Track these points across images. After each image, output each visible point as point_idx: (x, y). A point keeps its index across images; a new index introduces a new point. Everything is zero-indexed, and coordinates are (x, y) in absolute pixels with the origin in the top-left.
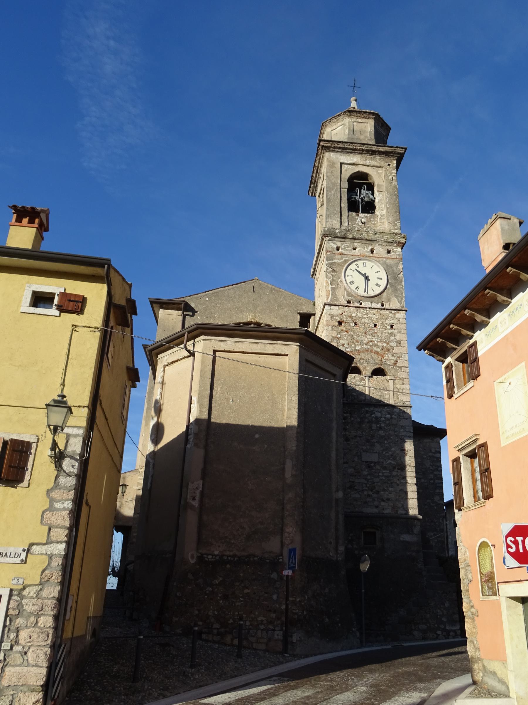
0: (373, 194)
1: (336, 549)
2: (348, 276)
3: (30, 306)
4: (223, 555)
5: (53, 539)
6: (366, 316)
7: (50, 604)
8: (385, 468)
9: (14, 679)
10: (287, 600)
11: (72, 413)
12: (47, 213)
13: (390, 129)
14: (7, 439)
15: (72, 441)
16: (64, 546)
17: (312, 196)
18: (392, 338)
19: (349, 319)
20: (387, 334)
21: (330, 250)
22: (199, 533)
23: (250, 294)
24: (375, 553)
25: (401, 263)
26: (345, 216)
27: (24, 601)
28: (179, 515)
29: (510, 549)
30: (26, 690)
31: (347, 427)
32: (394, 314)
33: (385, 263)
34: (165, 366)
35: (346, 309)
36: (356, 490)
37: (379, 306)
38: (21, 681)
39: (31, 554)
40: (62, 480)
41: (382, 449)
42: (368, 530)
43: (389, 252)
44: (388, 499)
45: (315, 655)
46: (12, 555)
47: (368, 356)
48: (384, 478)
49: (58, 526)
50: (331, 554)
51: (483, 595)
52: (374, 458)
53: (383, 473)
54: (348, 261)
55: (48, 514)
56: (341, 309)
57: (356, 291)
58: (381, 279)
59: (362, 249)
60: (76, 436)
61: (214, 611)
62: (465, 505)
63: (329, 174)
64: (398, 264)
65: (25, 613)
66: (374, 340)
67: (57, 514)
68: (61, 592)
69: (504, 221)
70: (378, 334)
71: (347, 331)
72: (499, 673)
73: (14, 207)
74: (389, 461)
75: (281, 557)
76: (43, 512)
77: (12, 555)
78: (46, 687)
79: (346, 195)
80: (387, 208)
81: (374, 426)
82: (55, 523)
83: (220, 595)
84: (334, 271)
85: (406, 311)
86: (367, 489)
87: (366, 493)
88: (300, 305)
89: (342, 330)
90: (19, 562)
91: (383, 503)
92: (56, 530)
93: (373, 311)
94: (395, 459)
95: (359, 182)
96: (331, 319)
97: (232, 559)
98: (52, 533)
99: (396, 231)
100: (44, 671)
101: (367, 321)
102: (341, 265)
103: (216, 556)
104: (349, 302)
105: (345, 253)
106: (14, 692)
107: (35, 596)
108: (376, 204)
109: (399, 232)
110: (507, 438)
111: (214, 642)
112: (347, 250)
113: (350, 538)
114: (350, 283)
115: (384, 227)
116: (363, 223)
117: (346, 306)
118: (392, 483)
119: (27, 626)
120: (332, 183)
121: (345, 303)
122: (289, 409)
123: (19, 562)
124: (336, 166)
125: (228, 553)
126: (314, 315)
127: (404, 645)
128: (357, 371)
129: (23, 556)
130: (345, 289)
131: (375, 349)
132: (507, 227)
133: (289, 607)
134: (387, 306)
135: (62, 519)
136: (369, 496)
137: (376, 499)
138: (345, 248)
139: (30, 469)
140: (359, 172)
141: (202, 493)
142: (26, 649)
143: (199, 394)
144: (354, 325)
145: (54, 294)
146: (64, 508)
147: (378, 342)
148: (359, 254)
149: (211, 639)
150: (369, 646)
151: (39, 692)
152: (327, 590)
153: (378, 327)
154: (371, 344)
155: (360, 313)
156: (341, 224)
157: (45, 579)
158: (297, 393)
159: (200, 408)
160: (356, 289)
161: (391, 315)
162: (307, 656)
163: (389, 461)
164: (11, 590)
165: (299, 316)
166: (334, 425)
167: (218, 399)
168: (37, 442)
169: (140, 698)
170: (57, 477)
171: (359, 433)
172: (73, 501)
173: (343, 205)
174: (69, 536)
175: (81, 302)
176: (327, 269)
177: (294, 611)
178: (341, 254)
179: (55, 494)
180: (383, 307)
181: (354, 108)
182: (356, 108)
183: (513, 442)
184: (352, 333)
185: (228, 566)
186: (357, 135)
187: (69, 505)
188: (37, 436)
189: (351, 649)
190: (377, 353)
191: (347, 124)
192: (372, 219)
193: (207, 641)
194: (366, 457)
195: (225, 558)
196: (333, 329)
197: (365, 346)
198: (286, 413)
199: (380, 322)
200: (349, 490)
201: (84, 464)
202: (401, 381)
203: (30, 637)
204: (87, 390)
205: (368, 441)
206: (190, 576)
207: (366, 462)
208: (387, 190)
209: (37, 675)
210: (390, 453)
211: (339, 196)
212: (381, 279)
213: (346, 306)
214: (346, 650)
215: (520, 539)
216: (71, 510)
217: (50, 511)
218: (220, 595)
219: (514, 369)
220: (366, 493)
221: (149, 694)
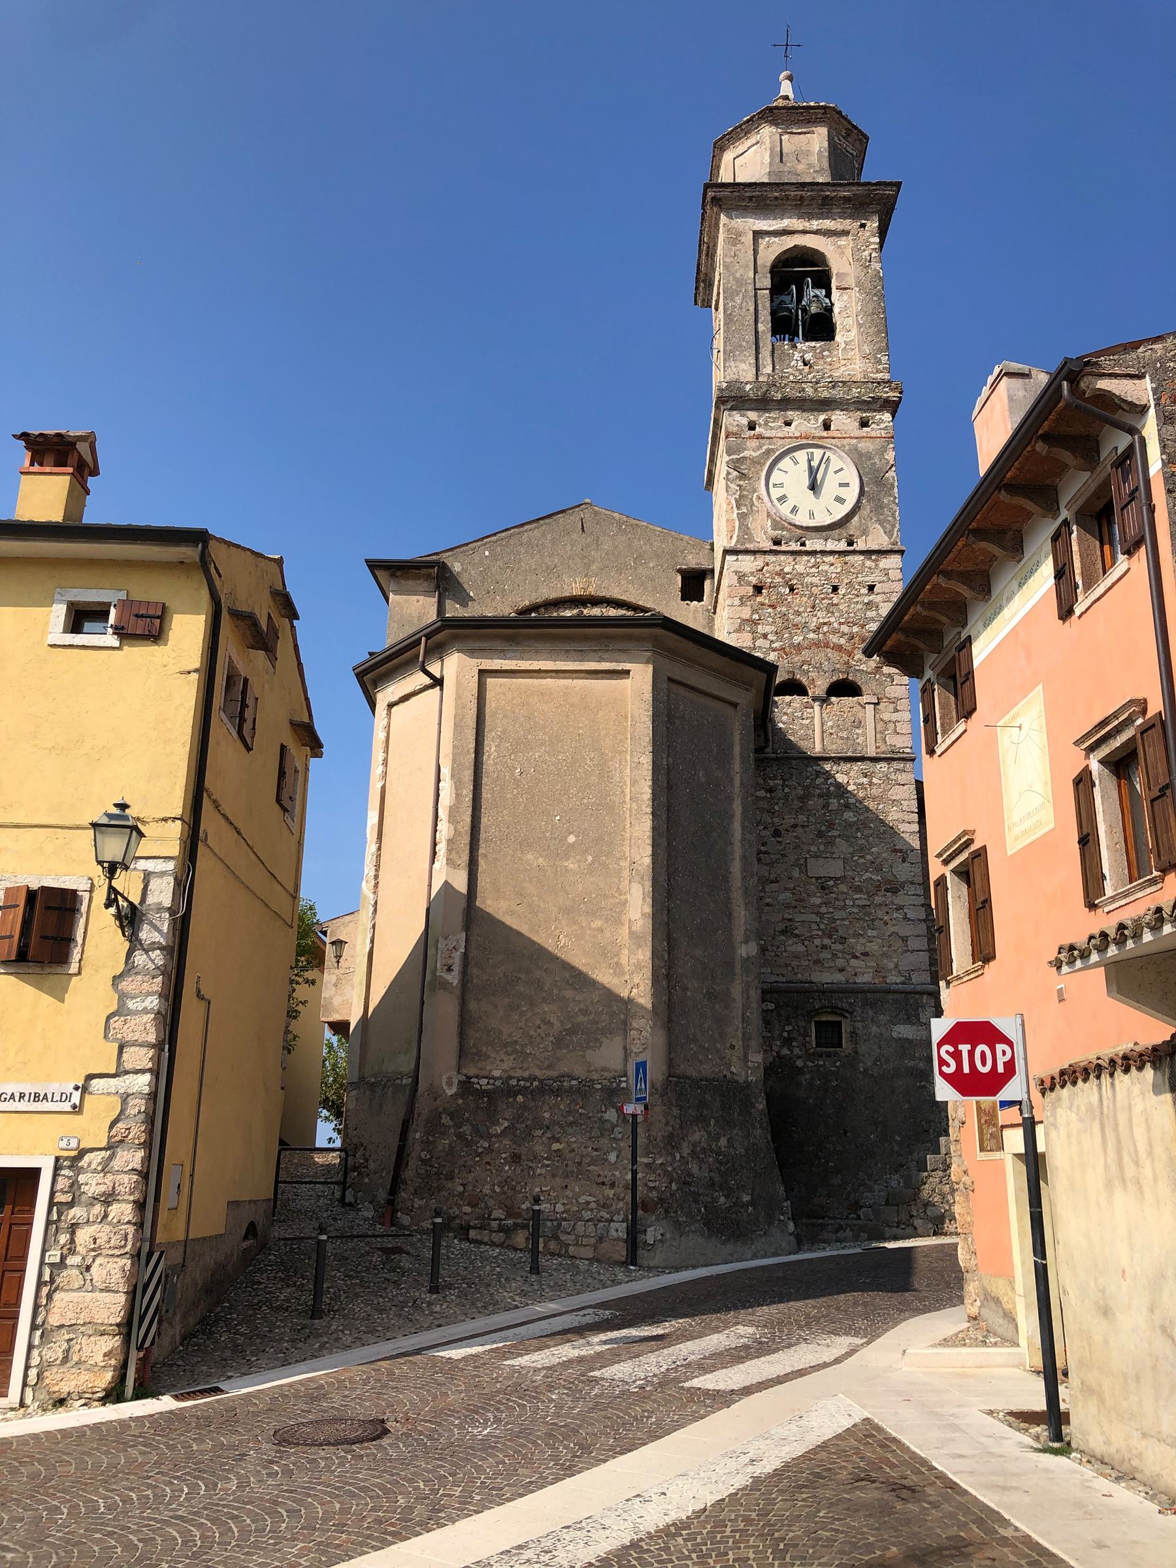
0: (829, 295)
1: (745, 1059)
2: (775, 485)
3: (65, 632)
4: (510, 1078)
5: (128, 1066)
6: (814, 570)
7: (126, 1181)
8: (858, 889)
9: (70, 1315)
10: (634, 1160)
11: (141, 835)
12: (90, 439)
13: (867, 139)
14: (35, 886)
15: (154, 884)
16: (147, 1078)
17: (703, 306)
18: (869, 614)
19: (778, 579)
20: (860, 606)
21: (735, 429)
22: (462, 1035)
23: (575, 536)
24: (838, 1064)
25: (892, 446)
26: (765, 353)
27: (82, 1178)
28: (423, 1003)
29: (944, 1069)
30: (90, 1332)
31: (776, 808)
32: (876, 560)
33: (856, 449)
34: (391, 706)
35: (771, 558)
36: (797, 936)
37: (842, 546)
38: (82, 1316)
39: (91, 1093)
40: (140, 958)
41: (851, 850)
42: (824, 1018)
43: (864, 424)
44: (866, 954)
45: (694, 1267)
46: (57, 1098)
47: (819, 656)
48: (856, 911)
49: (135, 1044)
50: (733, 1069)
51: (981, 1150)
52: (834, 868)
53: (854, 900)
54: (773, 451)
55: (116, 1023)
56: (760, 561)
57: (792, 516)
58: (847, 485)
59: (804, 424)
60: (162, 874)
61: (494, 1185)
62: (955, 974)
63: (728, 260)
64: (883, 450)
65: (84, 1198)
66: (832, 620)
67: (134, 1021)
68: (147, 1159)
69: (1017, 383)
70: (841, 607)
71: (773, 607)
72: (1004, 1300)
73: (24, 436)
74: (868, 875)
75: (624, 1079)
76: (109, 1018)
77: (57, 1098)
78: (126, 1328)
79: (768, 304)
80: (860, 326)
81: (834, 804)
82: (130, 1037)
83: (504, 1156)
84: (743, 476)
85: (902, 552)
86: (820, 933)
87: (817, 942)
88: (682, 552)
89: (763, 604)
90: (70, 1109)
91: (853, 962)
92: (132, 1049)
93: (830, 559)
94: (879, 870)
95: (798, 273)
96: (739, 582)
97: (528, 1084)
98: (125, 1056)
99: (879, 376)
100: (121, 1299)
101: (815, 580)
102: (757, 462)
103: (495, 1079)
104: (777, 542)
105: (768, 434)
106: (72, 1336)
107: (100, 1168)
108: (837, 317)
109: (887, 376)
110: (1016, 839)
111: (493, 1244)
112: (772, 428)
113: (785, 1034)
114: (779, 499)
115: (853, 369)
116: (805, 364)
117: (771, 552)
118: (873, 920)
119: (88, 1221)
120: (735, 279)
121: (768, 545)
122: (634, 783)
123: (70, 1109)
124: (743, 239)
125: (519, 1073)
126: (712, 571)
127: (891, 1245)
128: (795, 688)
129: (76, 1098)
130: (769, 515)
131: (834, 639)
132: (1021, 393)
133: (639, 1176)
134: (860, 545)
135: (143, 1027)
136: (824, 947)
137: (840, 955)
138: (766, 424)
139: (79, 939)
140: (795, 246)
141: (465, 956)
142: (89, 1261)
143: (454, 761)
144: (788, 590)
145: (109, 604)
146: (145, 1008)
147: (840, 624)
148: (797, 435)
149: (486, 1239)
150: (810, 1250)
151: (114, 1336)
152: (723, 1142)
153: (842, 591)
154: (825, 629)
155: (802, 565)
156: (757, 370)
157: (117, 1139)
158: (651, 749)
159: (456, 789)
160: (792, 512)
161: (868, 563)
162: (677, 1269)
163: (868, 875)
164: (57, 1159)
165: (679, 578)
166: (737, 807)
167: (491, 769)
168: (91, 891)
169: (317, 1346)
170: (129, 954)
171: (802, 818)
172: (160, 996)
173: (761, 327)
174: (157, 1060)
175: (158, 617)
176: (728, 473)
177: (651, 1184)
178: (759, 437)
179: (126, 985)
180: (851, 548)
181: (786, 98)
182: (791, 96)
183: (1023, 848)
184: (784, 609)
185: (520, 1098)
186: (790, 163)
187: (153, 1002)
188: (90, 879)
189: (775, 1255)
190: (839, 648)
191: (767, 141)
192: (826, 353)
193: (480, 1243)
194: (817, 868)
195: (513, 1082)
196: (742, 604)
197: (811, 635)
198: (628, 791)
199: (846, 581)
200: (783, 938)
201: (182, 926)
202: (892, 706)
203: (95, 1240)
204: (178, 786)
205: (820, 834)
206: (445, 1120)
207: (817, 878)
208: (859, 284)
209: (110, 1307)
210: (869, 857)
211: (752, 308)
212: (847, 485)
213: (771, 552)
214: (765, 1256)
215: (965, 1048)
216: (159, 1013)
217: (120, 1016)
218: (504, 1156)
219: (1031, 695)
220: (817, 942)
221: (337, 1340)
